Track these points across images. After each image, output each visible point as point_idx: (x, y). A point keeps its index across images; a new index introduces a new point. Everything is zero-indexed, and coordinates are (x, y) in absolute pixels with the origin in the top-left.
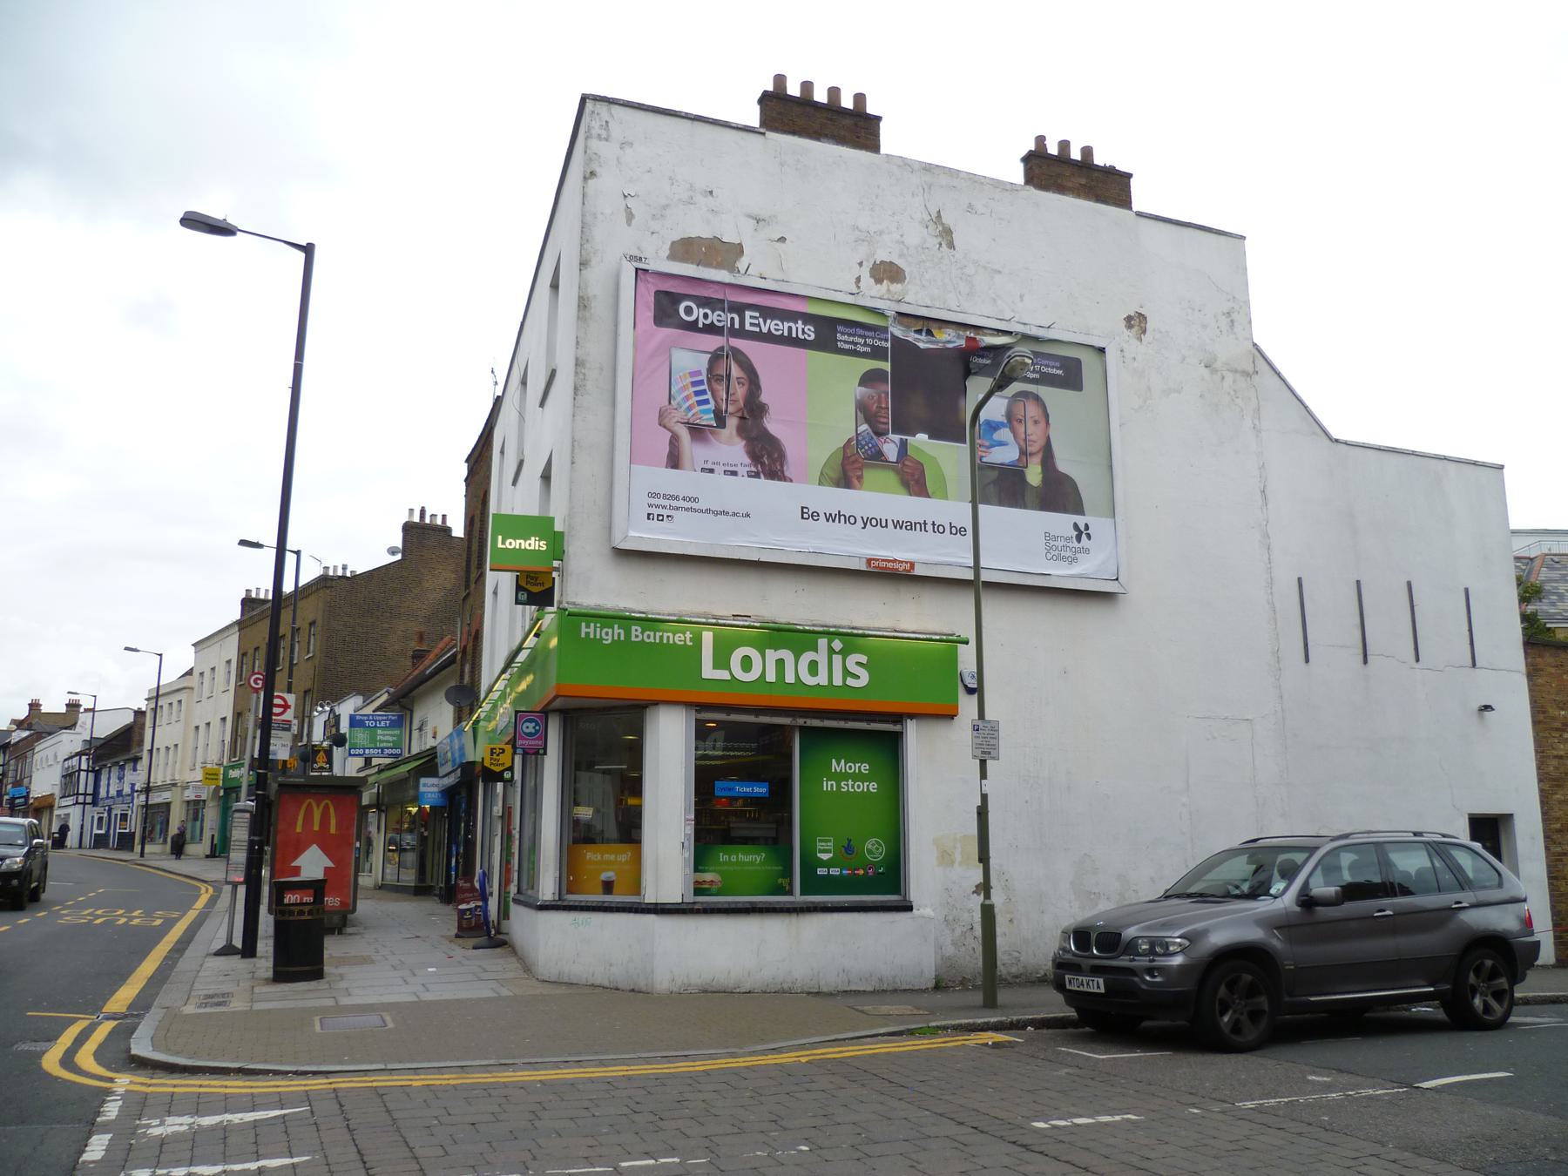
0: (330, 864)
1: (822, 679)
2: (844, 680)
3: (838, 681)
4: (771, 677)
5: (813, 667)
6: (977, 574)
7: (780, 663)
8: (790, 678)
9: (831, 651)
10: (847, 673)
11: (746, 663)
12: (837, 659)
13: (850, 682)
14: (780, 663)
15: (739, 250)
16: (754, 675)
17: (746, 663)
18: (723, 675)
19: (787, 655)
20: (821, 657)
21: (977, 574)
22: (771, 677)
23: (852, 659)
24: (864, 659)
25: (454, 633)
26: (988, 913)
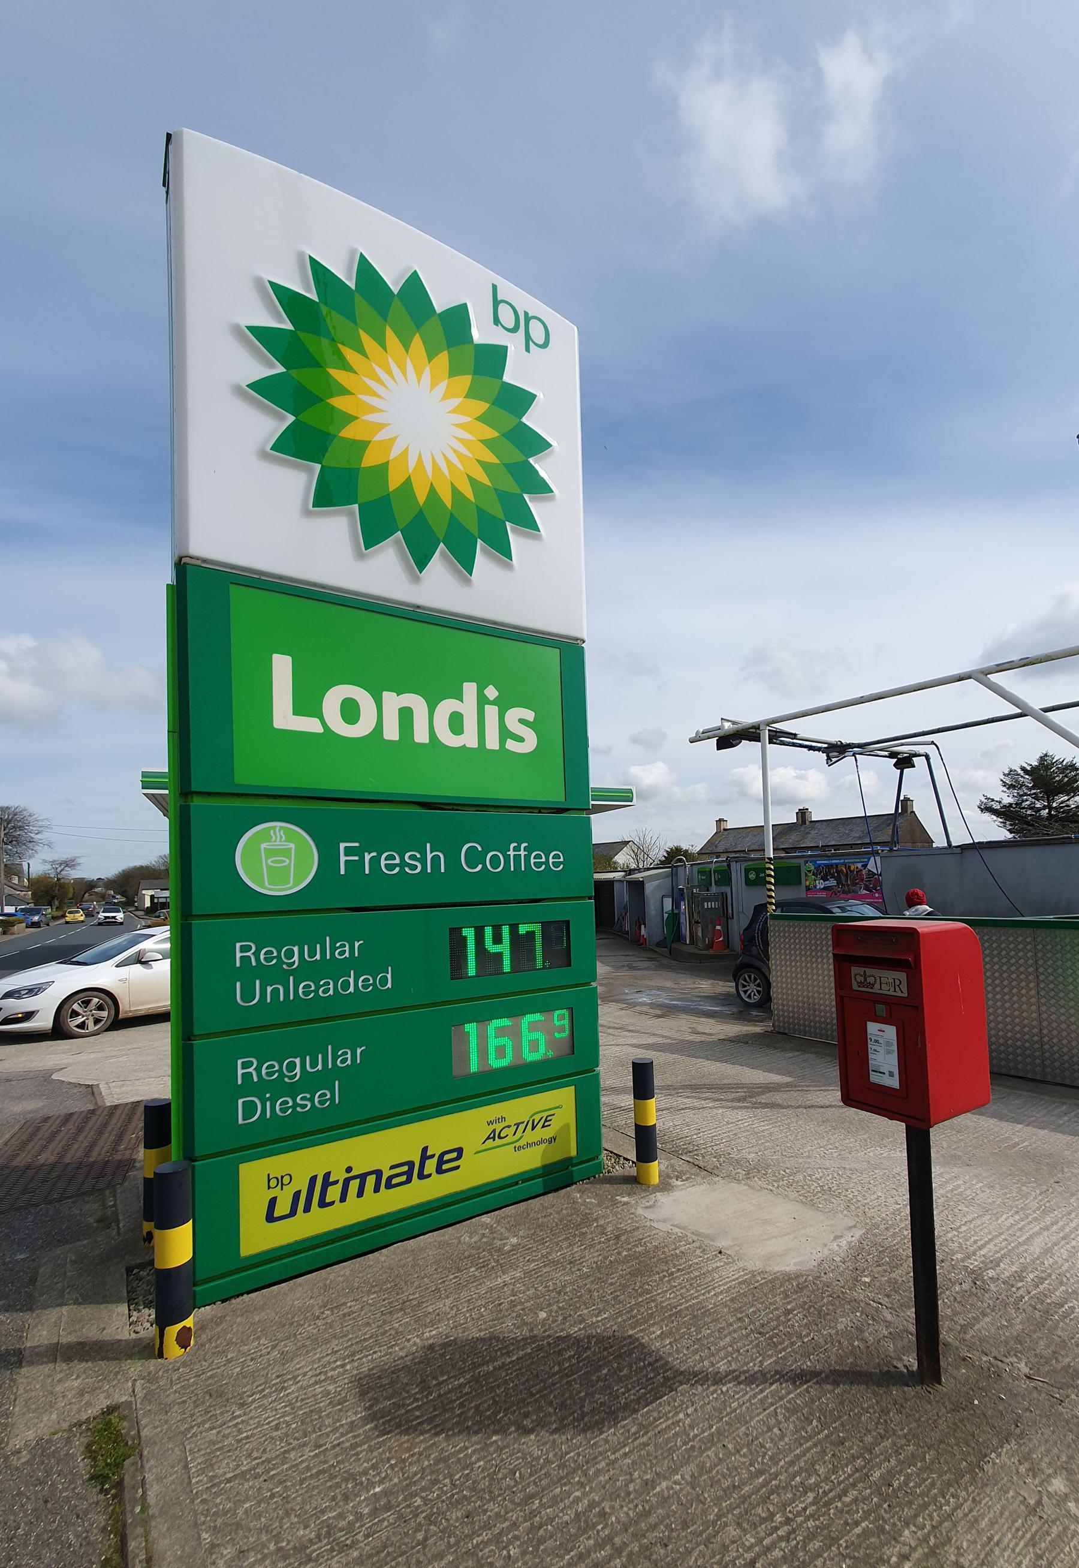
0: (934, 845)
1: (469, 739)
2: (502, 742)
3: (492, 742)
4: (392, 732)
5: (456, 723)
6: (865, 980)
7: (406, 716)
8: (421, 736)
9: (482, 701)
10: (505, 734)
11: (350, 711)
12: (492, 713)
13: (511, 745)
14: (406, 716)
15: (720, 747)
16: (363, 728)
17: (350, 711)
18: (310, 725)
19: (417, 703)
20: (468, 706)
21: (865, 980)
22: (392, 732)
23: (514, 715)
24: (529, 715)
25: (837, 865)
26: (781, 1376)
